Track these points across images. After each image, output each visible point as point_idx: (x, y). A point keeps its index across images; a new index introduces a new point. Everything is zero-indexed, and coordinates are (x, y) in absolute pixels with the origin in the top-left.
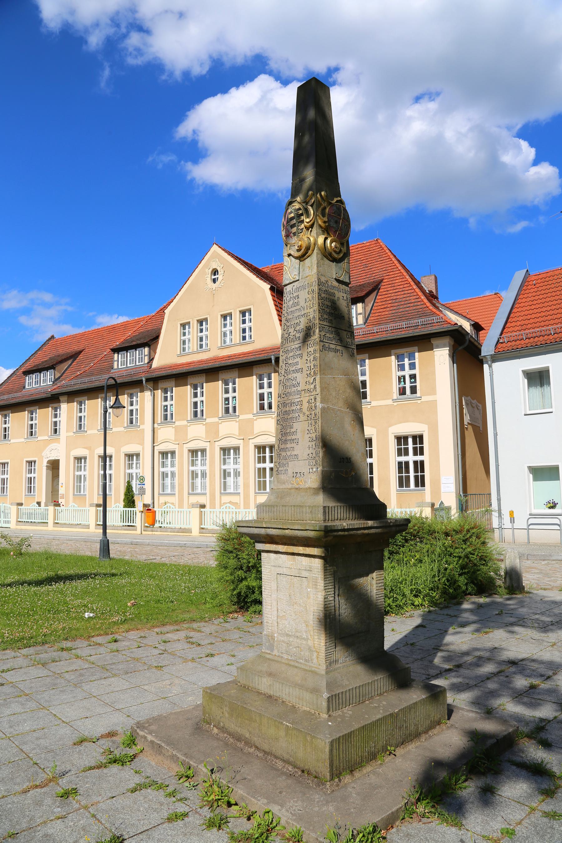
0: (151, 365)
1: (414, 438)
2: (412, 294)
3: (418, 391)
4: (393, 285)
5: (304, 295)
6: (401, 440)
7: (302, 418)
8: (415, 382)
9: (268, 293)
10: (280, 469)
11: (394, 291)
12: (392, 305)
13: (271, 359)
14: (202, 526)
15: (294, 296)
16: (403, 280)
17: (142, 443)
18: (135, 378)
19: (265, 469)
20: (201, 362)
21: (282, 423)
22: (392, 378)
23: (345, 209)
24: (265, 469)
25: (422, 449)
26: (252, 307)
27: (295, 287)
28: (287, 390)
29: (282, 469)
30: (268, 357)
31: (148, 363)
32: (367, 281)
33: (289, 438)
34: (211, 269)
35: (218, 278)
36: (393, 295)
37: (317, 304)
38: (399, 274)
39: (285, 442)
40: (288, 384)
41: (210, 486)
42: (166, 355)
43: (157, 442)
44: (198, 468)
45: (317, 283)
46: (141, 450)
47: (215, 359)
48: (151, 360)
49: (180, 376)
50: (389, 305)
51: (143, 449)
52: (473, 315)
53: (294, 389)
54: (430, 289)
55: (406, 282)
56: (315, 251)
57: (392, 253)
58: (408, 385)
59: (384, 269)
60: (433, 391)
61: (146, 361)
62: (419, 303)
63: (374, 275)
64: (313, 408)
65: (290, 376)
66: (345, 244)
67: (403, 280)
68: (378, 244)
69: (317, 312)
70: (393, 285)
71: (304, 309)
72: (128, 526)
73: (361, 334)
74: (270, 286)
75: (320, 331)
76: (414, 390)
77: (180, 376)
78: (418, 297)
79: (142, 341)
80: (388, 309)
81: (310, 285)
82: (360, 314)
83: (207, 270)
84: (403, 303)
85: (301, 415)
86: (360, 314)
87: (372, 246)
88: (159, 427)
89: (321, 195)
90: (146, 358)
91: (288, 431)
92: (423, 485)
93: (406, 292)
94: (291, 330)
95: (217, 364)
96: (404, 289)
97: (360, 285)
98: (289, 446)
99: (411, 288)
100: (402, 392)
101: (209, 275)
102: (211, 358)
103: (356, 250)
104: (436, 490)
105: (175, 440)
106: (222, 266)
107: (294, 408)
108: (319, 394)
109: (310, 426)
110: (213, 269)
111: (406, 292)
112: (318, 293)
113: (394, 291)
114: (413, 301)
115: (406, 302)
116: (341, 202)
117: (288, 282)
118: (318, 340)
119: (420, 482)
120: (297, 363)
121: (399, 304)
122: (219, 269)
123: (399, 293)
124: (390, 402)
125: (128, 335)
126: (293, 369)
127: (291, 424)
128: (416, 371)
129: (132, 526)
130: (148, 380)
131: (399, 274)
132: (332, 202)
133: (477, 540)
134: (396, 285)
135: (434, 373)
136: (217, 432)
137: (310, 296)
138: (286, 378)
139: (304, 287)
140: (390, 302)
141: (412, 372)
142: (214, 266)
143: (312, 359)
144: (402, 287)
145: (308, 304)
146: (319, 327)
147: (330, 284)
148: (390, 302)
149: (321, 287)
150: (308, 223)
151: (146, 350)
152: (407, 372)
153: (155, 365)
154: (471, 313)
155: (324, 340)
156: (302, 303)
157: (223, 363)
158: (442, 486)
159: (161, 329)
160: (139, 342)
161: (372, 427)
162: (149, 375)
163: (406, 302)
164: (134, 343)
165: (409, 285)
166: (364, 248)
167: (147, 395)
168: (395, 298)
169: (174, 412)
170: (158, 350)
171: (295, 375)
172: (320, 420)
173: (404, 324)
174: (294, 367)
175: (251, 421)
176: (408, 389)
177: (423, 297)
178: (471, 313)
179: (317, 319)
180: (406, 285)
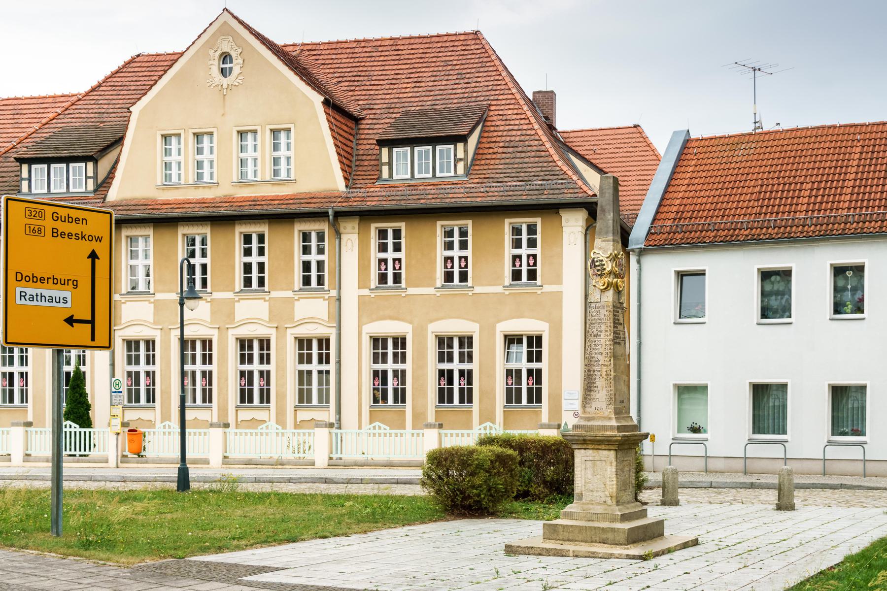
1: (530, 338)
3: (539, 277)
5: (603, 312)
6: (512, 340)
8: (535, 264)
9: (320, 109)
12: (505, 150)
13: (328, 213)
14: (28, 452)
19: (309, 373)
20: (202, 202)
24: (309, 373)
26: (292, 126)
30: (324, 210)
34: (219, 53)
35: (231, 69)
41: (219, 396)
47: (230, 201)
50: (500, 150)
52: (602, 161)
57: (502, 64)
59: (490, 88)
60: (558, 280)
63: (475, 95)
68: (478, 41)
70: (504, 118)
72: (70, 455)
74: (322, 98)
78: (541, 143)
80: (499, 156)
83: (211, 52)
88: (123, 300)
92: (539, 400)
96: (521, 127)
99: (530, 126)
101: (216, 62)
104: (556, 410)
105: (155, 323)
106: (240, 50)
110: (223, 53)
114: (534, 148)
119: (535, 396)
124: (499, 289)
128: (537, 251)
129: (85, 456)
131: (513, 101)
133: (150, 508)
135: (560, 255)
136: (231, 315)
139: (603, 307)
142: (226, 48)
148: (501, 144)
151: (90, 165)
153: (114, 194)
154: (599, 152)
156: (602, 316)
158: (564, 402)
161: (473, 321)
165: (527, 122)
166: (456, 44)
168: (508, 139)
175: (290, 302)
176: (524, 273)
178: (599, 152)
180: (522, 122)
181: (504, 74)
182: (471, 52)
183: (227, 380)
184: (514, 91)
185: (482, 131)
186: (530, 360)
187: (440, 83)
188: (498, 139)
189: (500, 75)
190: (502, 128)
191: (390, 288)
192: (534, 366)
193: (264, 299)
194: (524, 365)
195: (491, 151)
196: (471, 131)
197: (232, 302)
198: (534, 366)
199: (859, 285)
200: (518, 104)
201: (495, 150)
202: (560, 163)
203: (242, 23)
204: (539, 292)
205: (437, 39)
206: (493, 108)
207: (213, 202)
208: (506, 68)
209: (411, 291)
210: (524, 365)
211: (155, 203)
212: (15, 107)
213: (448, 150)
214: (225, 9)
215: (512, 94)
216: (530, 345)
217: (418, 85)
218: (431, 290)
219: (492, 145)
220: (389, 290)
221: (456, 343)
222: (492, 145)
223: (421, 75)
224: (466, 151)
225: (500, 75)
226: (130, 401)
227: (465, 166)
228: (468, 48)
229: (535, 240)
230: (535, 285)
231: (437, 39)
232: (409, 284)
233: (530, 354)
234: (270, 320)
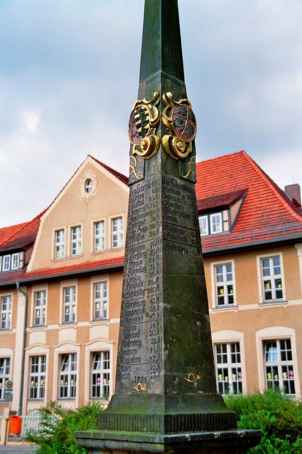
0: (26, 270)
1: (282, 342)
2: (275, 203)
4: (257, 194)
6: (268, 344)
7: (145, 319)
10: (122, 373)
11: (259, 199)
12: (257, 213)
15: (139, 194)
16: (267, 189)
17: (13, 348)
18: (9, 283)
20: (74, 267)
21: (125, 324)
22: (257, 283)
23: (191, 110)
25: (290, 354)
27: (141, 186)
28: (131, 290)
29: (124, 373)
31: (23, 268)
32: (233, 190)
33: (132, 340)
34: (85, 179)
35: (91, 188)
36: (257, 203)
37: (161, 202)
38: (263, 184)
39: (128, 344)
40: (132, 283)
42: (39, 261)
43: (29, 346)
44: (68, 372)
45: (161, 182)
46: (12, 354)
47: (87, 265)
48: (25, 265)
49: (53, 280)
50: (254, 213)
51: (14, 353)
53: (139, 288)
54: (293, 198)
55: (270, 191)
56: (160, 150)
58: (273, 290)
61: (21, 266)
62: (283, 211)
64: (156, 308)
65: (133, 276)
66: (191, 144)
67: (267, 189)
68: (242, 156)
69: (161, 210)
70: (257, 194)
71: (148, 207)
73: (227, 240)
75: (163, 229)
76: (279, 294)
77: (53, 280)
78: (281, 205)
79: (18, 246)
81: (154, 183)
82: (226, 221)
83: (81, 180)
84: (267, 211)
85: (144, 316)
86: (226, 221)
87: (237, 158)
88: (31, 331)
89: (166, 97)
90: (21, 263)
91: (131, 333)
93: (270, 200)
94: (136, 229)
95: (89, 270)
96: (268, 198)
97: (226, 194)
98: (131, 348)
99: (274, 196)
100: (268, 296)
101: (83, 185)
102: (83, 263)
103: (222, 162)
107: (136, 308)
108: (162, 294)
109: (153, 327)
111: (270, 200)
112: (162, 192)
113: (259, 199)
114: (277, 209)
115: (270, 210)
116: (187, 103)
117: (133, 181)
118: (161, 238)
120: (141, 262)
121: (264, 211)
122: (92, 179)
123: (263, 202)
124: (255, 306)
125: (4, 241)
126: (136, 268)
127: (134, 325)
130: (22, 284)
132: (178, 103)
134: (260, 193)
136: (87, 336)
137: (154, 195)
138: (130, 277)
140: (255, 210)
141: (278, 277)
142: (88, 177)
143: (155, 258)
144: (266, 195)
145: (152, 202)
146: (163, 226)
147: (175, 183)
148: (255, 210)
149: (165, 185)
150: (152, 123)
151: (22, 254)
152: (272, 277)
153: (30, 269)
155: (168, 239)
156: (146, 202)
157: (95, 268)
159: (35, 235)
160: (14, 248)
162: (23, 280)
163: (270, 210)
164: (10, 249)
167: (21, 298)
168: (259, 206)
169: (46, 316)
170: (33, 256)
171: (139, 274)
172: (162, 320)
173: (267, 230)
174: (138, 266)
177: (286, 205)
179: (161, 216)
180: (269, 194)
181: (251, 162)
182: (238, 162)
183: (84, 380)
184: (263, 178)
185: (242, 204)
186: (283, 359)
187: (218, 182)
188: (253, 207)
189: (255, 171)
190: (255, 200)
191: (226, 307)
192: (287, 363)
193: (73, 327)
194: (279, 363)
195: (247, 214)
196: (233, 203)
197: (88, 328)
198: (287, 363)
199: (99, 318)
200: (266, 185)
201: (250, 214)
202: (294, 215)
203: (102, 165)
204: (285, 306)
205: (219, 160)
206: (249, 190)
207: (79, 266)
208: (259, 167)
209: (291, 303)
210: (279, 363)
211: (50, 271)
212: (5, 230)
213: (218, 217)
214: (89, 155)
215: (263, 180)
216: (282, 347)
217: (205, 185)
218: (255, 306)
219: (248, 211)
220: (274, 304)
221: (229, 348)
222: (248, 211)
223: (207, 180)
224: (229, 216)
225: (255, 171)
226: (32, 397)
227: (230, 224)
228: (236, 161)
229: (279, 268)
230: (233, 306)
231: (219, 160)
232: (239, 303)
233: (283, 354)
234: (77, 343)
